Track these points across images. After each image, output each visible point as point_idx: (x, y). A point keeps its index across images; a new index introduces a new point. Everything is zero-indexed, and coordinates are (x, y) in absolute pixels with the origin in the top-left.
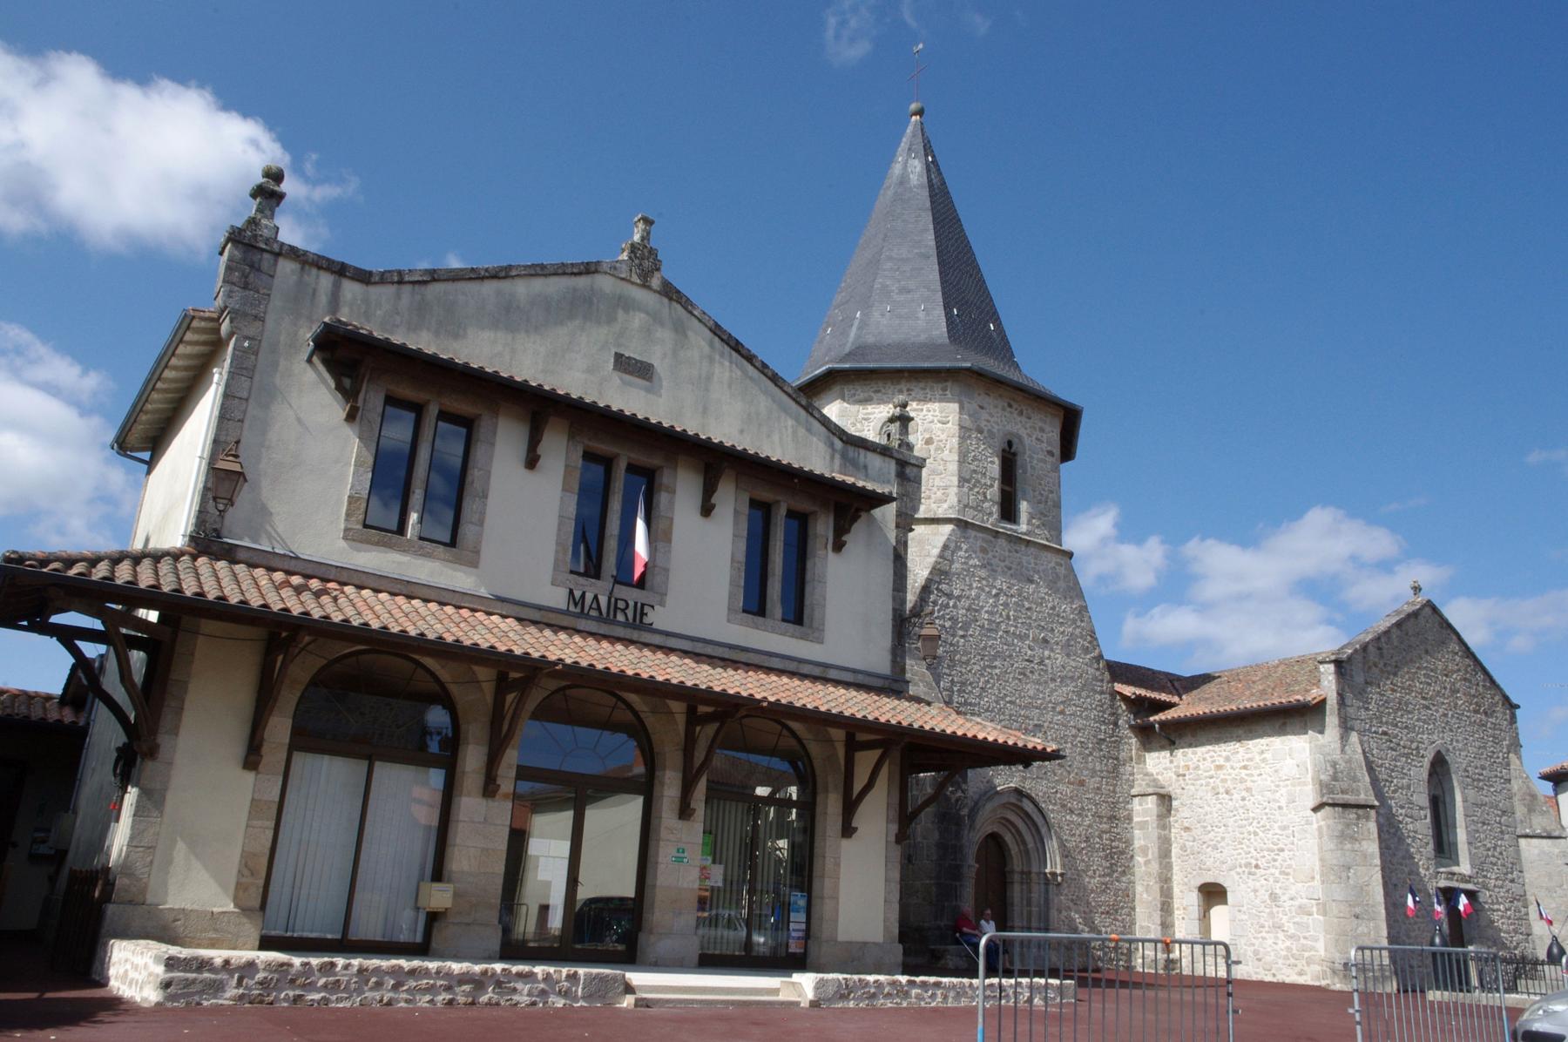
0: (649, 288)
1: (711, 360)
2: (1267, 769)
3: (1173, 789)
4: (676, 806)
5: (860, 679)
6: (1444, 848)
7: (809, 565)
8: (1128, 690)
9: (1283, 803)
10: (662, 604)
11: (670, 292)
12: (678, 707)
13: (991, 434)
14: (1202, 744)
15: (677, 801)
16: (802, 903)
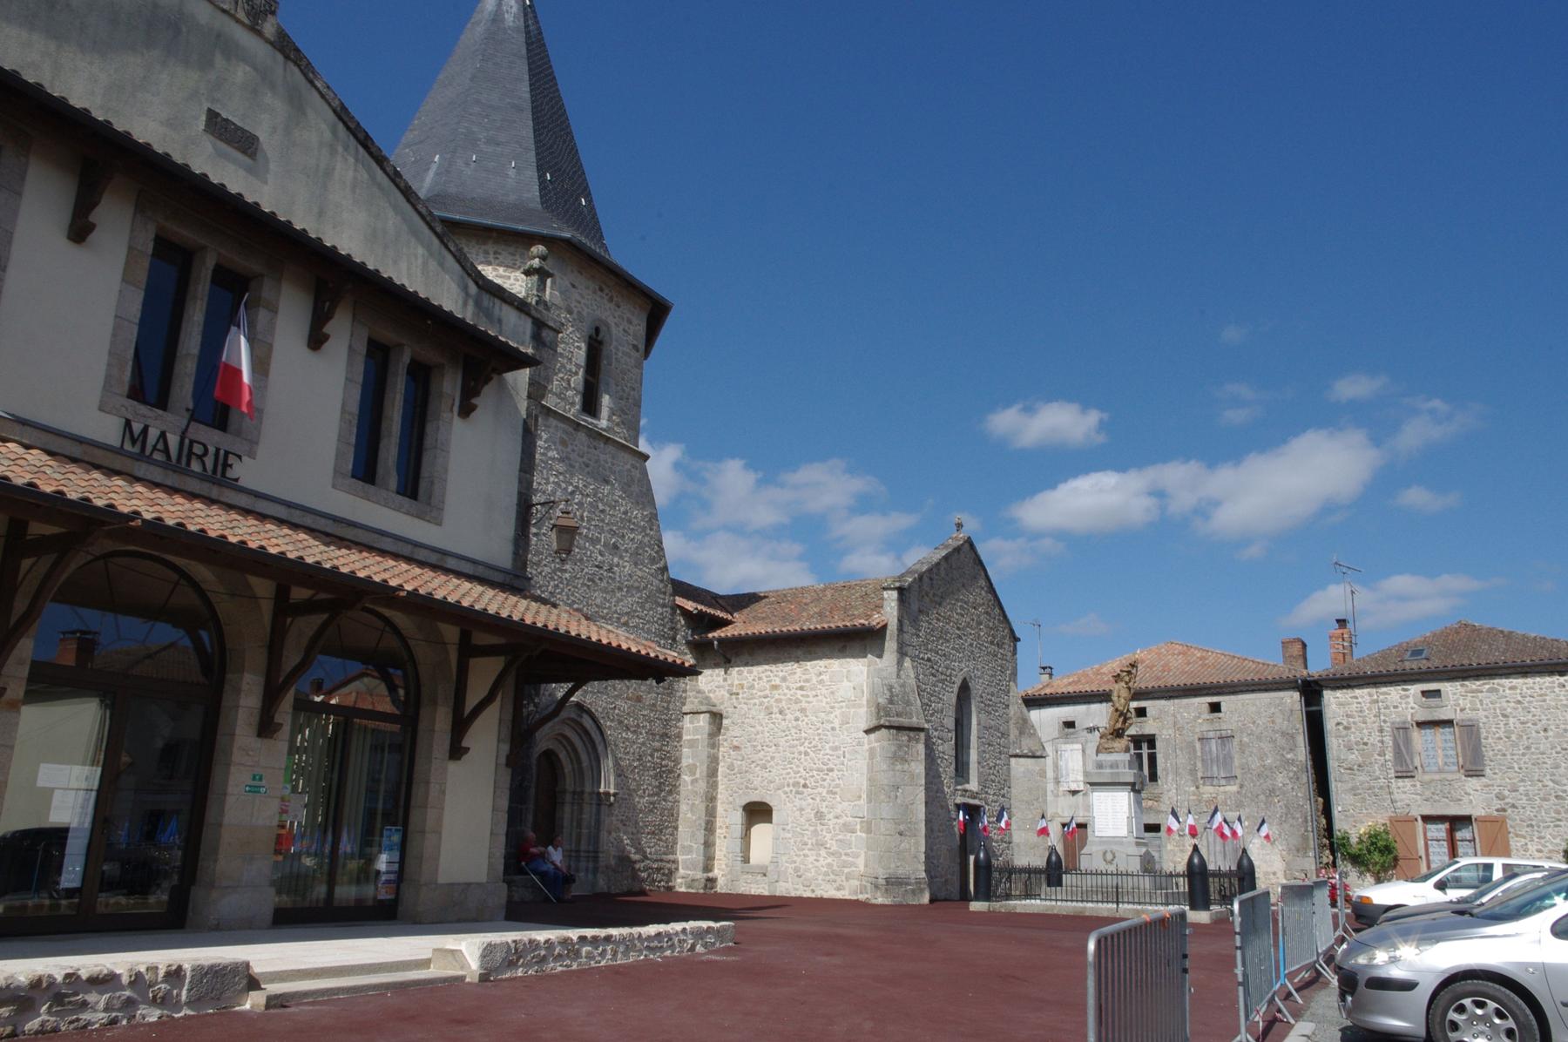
0: (259, 33)
1: (333, 152)
2: (824, 691)
3: (720, 708)
4: (255, 719)
5: (480, 571)
6: (961, 771)
7: (429, 428)
8: (690, 605)
9: (837, 725)
10: (252, 455)
11: (285, 46)
12: (263, 588)
13: (580, 318)
14: (759, 664)
15: (257, 713)
16: (396, 838)
